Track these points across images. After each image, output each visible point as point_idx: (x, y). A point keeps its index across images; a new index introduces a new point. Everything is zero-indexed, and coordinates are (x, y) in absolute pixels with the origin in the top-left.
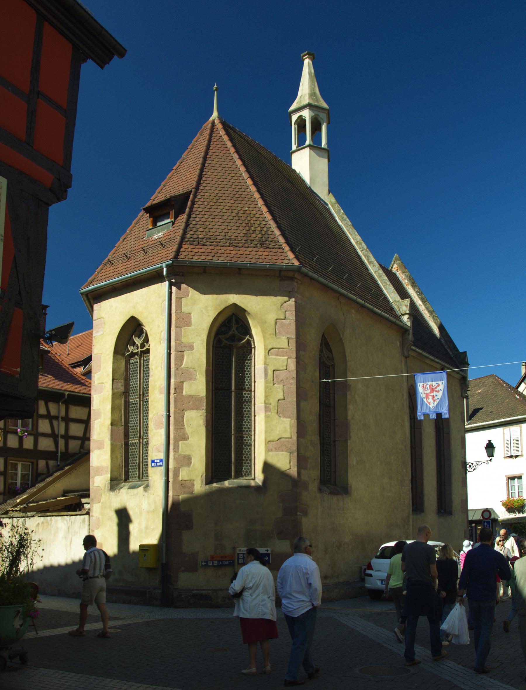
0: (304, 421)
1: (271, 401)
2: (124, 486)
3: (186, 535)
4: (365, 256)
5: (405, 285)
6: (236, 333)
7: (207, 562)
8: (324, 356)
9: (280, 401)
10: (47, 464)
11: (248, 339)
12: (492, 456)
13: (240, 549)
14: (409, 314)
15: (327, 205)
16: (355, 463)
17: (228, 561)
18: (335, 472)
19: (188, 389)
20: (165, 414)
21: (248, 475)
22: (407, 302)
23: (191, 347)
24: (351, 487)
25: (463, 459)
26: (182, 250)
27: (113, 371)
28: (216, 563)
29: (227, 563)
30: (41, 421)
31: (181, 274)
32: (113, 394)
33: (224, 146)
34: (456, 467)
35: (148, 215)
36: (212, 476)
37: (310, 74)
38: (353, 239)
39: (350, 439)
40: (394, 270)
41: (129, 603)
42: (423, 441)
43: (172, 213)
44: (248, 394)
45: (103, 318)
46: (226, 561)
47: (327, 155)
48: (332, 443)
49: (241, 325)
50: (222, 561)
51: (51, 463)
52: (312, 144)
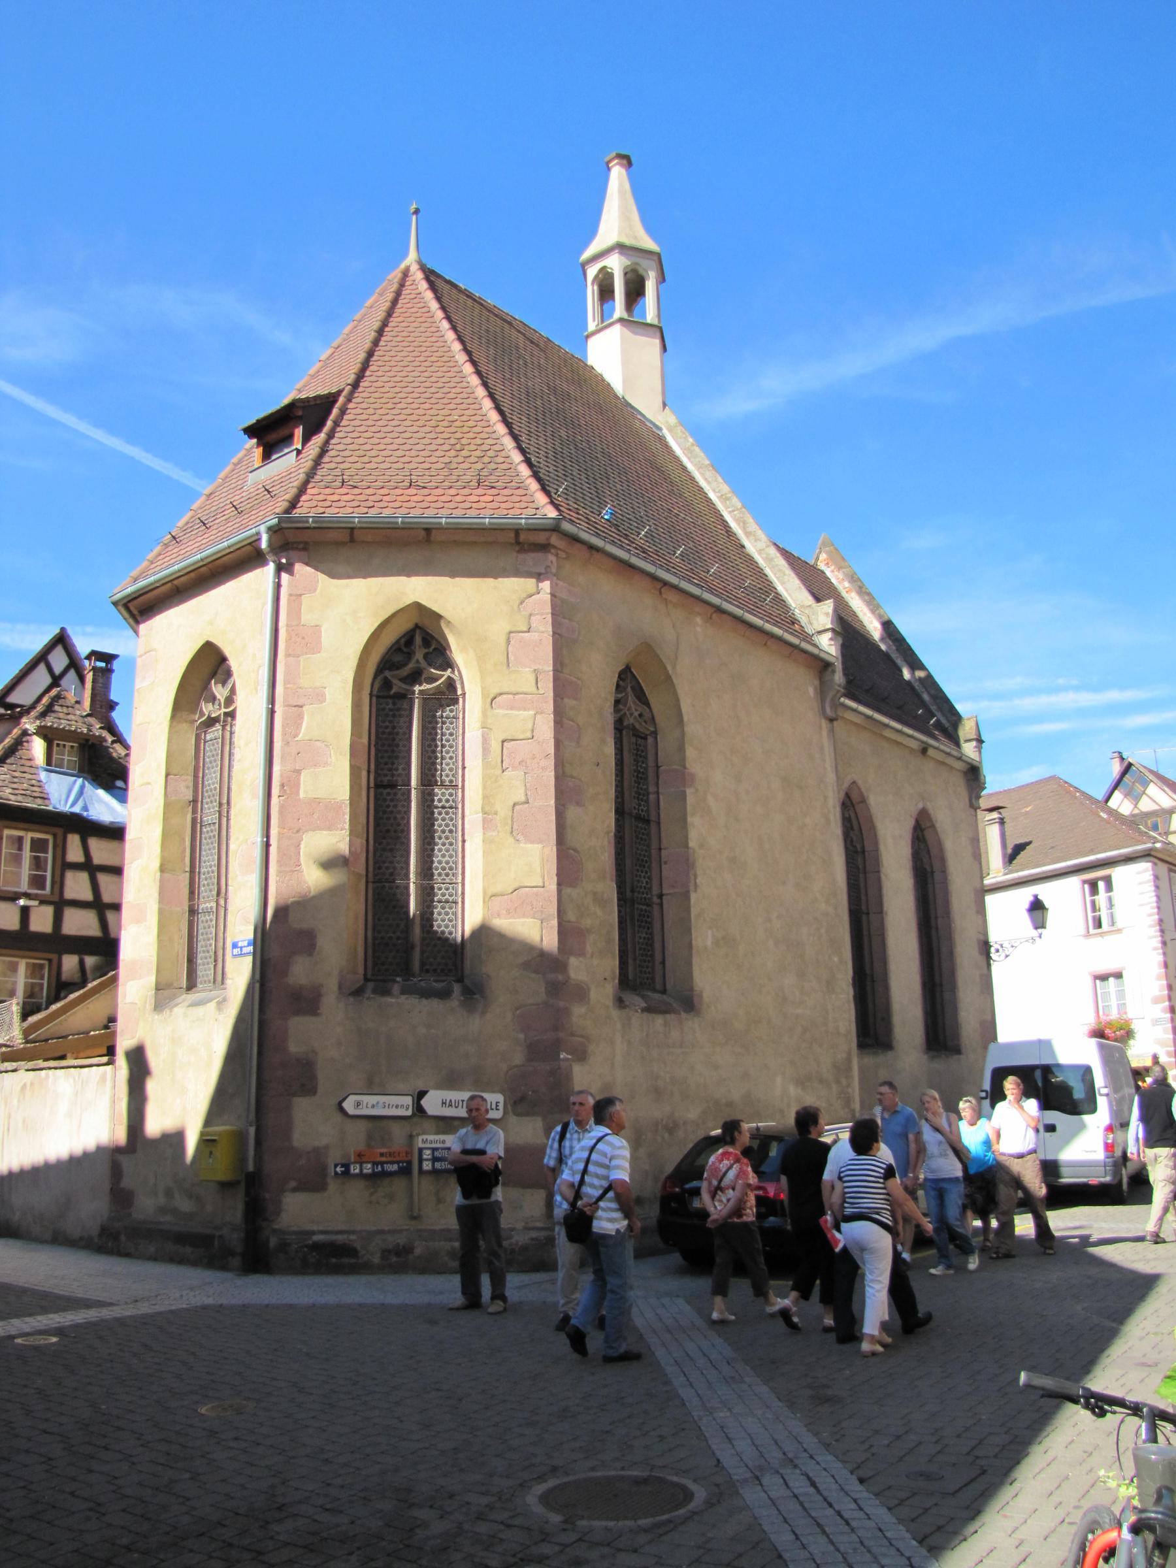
0: (575, 850)
1: (498, 807)
2: (184, 1000)
3: (302, 1107)
4: (737, 521)
5: (844, 594)
6: (423, 664)
7: (346, 1166)
8: (631, 714)
9: (517, 807)
10: (82, 963)
11: (449, 677)
12: (1043, 927)
13: (425, 1137)
14: (833, 630)
15: (660, 429)
16: (709, 943)
17: (398, 1163)
18: (663, 962)
19: (310, 786)
20: (259, 839)
22: (828, 606)
23: (319, 696)
24: (701, 996)
25: (982, 937)
26: (304, 498)
27: (167, 757)
28: (368, 1168)
29: (395, 1167)
30: (70, 876)
31: (301, 546)
32: (167, 805)
34: (965, 952)
35: (255, 441)
36: (365, 975)
37: (621, 192)
38: (714, 491)
39: (696, 891)
40: (821, 566)
41: (181, 1261)
42: (885, 899)
43: (299, 432)
44: (451, 795)
46: (392, 1163)
47: (658, 335)
48: (655, 900)
49: (435, 649)
50: (382, 1163)
51: (90, 961)
52: (626, 316)
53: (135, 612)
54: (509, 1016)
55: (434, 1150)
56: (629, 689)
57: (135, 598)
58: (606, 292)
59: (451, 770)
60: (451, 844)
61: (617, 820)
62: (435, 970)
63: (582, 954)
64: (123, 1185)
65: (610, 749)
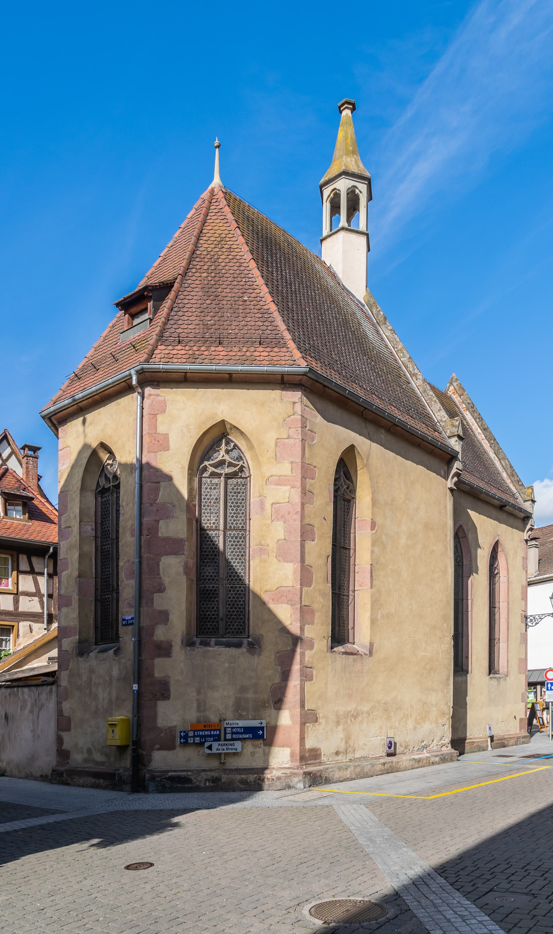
2: (95, 649)
3: (162, 707)
13: (227, 722)
18: (354, 627)
21: (241, 632)
33: (225, 221)
43: (150, 305)
45: (69, 447)
52: (346, 225)
53: (55, 422)
54: (273, 657)
55: (232, 728)
56: (342, 473)
57: (55, 414)
58: (335, 208)
59: (242, 520)
60: (242, 563)
61: (333, 549)
62: (233, 632)
63: (312, 623)
64: (63, 748)
65: (331, 508)
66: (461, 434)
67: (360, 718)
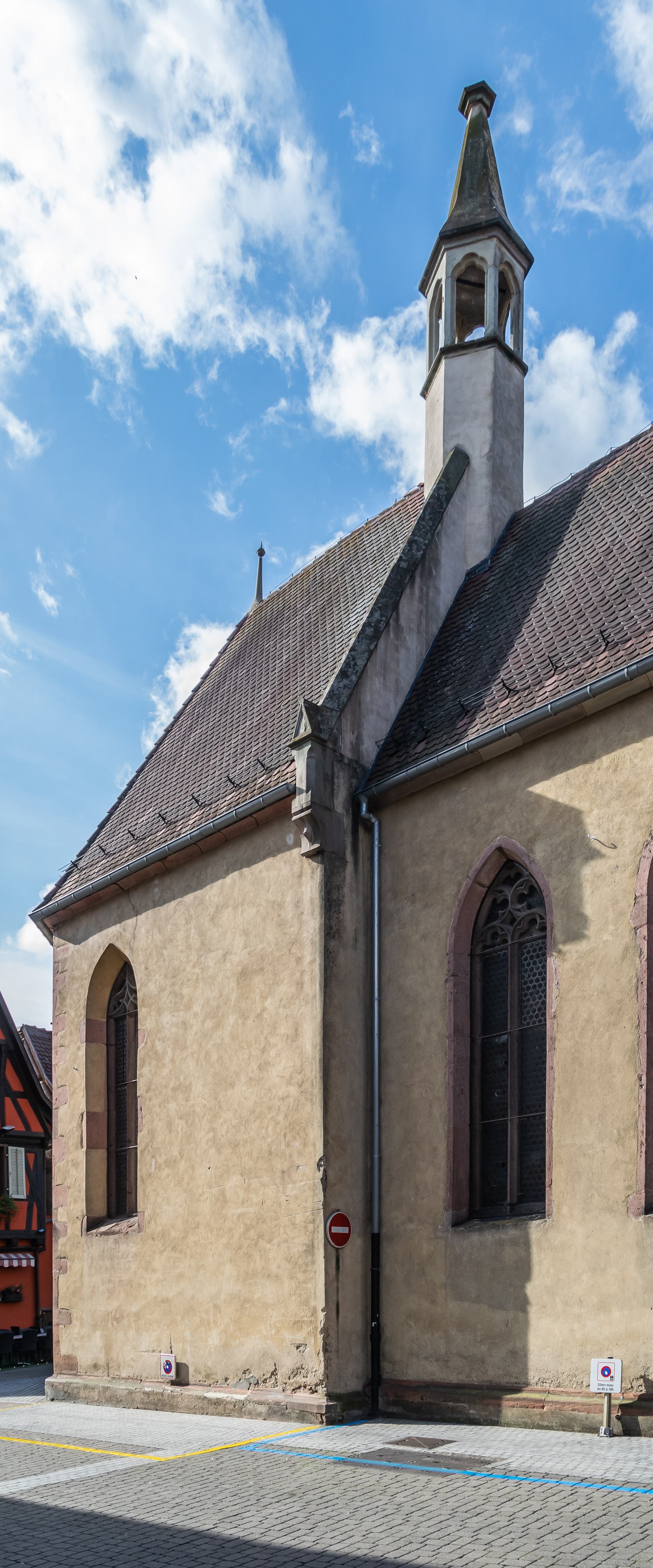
66: (498, 902)
67: (125, 1322)
